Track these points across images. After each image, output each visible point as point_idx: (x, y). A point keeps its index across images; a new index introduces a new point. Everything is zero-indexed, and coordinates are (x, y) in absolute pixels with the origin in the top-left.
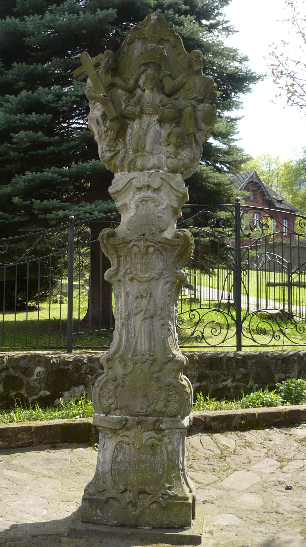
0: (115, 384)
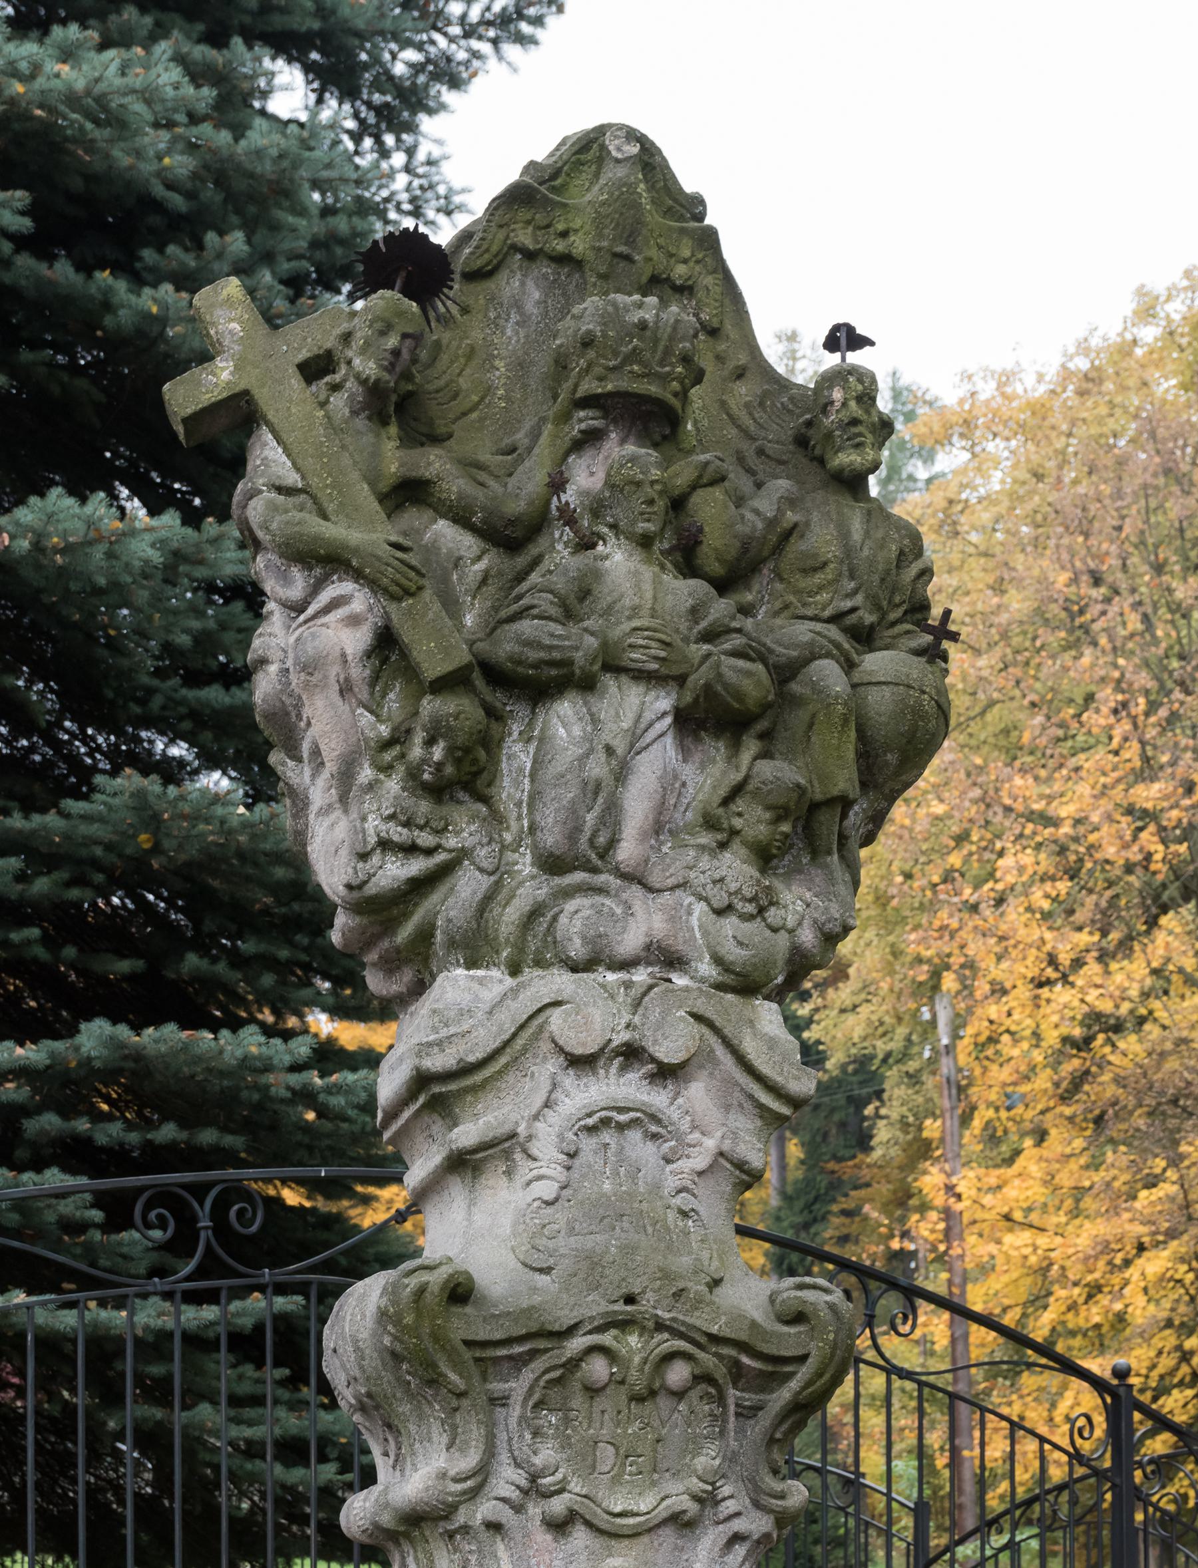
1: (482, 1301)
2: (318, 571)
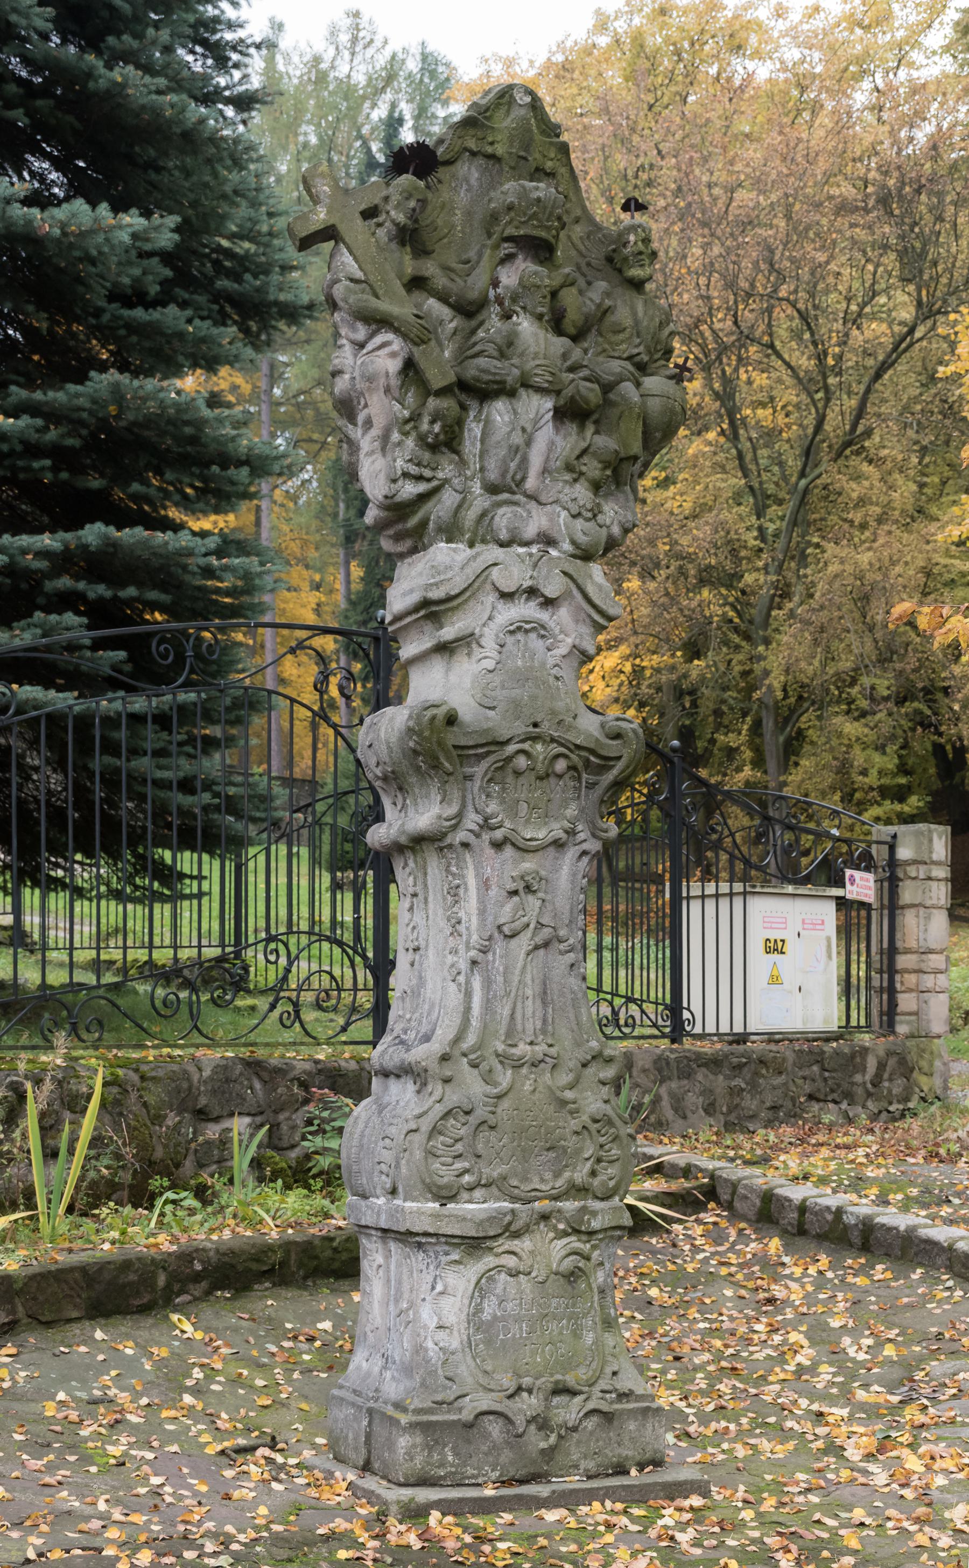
0: (473, 1120)
1: (461, 725)
2: (374, 327)
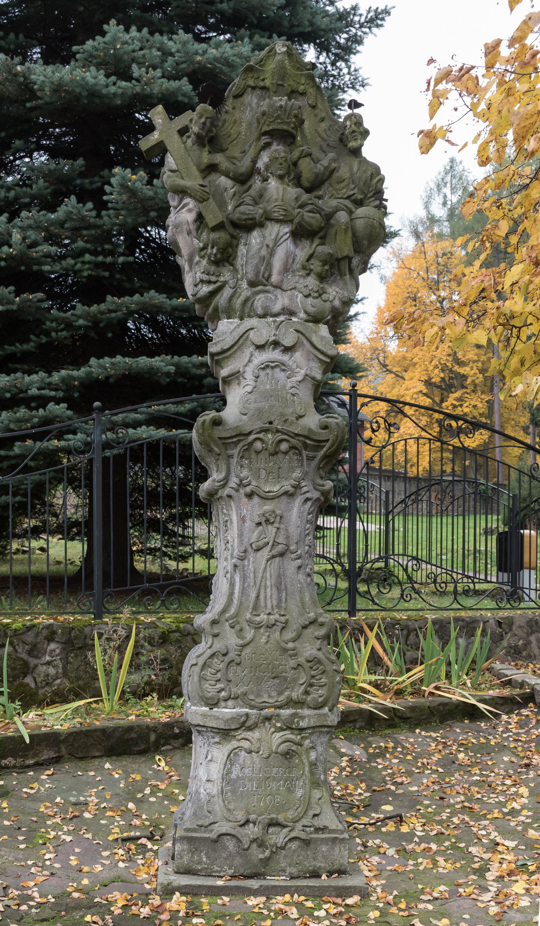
0: (227, 659)
